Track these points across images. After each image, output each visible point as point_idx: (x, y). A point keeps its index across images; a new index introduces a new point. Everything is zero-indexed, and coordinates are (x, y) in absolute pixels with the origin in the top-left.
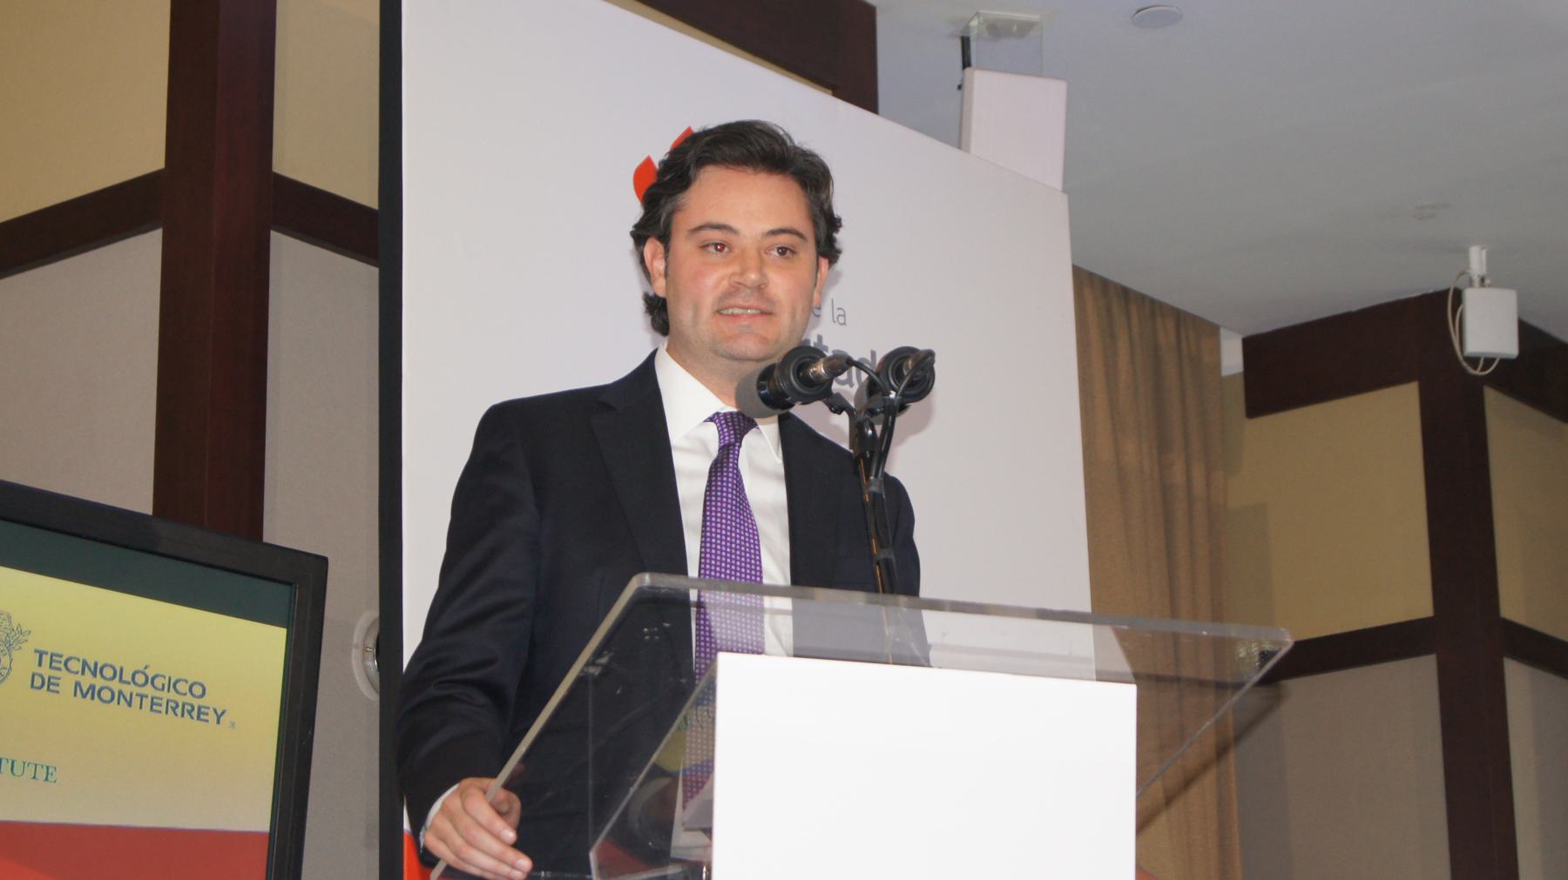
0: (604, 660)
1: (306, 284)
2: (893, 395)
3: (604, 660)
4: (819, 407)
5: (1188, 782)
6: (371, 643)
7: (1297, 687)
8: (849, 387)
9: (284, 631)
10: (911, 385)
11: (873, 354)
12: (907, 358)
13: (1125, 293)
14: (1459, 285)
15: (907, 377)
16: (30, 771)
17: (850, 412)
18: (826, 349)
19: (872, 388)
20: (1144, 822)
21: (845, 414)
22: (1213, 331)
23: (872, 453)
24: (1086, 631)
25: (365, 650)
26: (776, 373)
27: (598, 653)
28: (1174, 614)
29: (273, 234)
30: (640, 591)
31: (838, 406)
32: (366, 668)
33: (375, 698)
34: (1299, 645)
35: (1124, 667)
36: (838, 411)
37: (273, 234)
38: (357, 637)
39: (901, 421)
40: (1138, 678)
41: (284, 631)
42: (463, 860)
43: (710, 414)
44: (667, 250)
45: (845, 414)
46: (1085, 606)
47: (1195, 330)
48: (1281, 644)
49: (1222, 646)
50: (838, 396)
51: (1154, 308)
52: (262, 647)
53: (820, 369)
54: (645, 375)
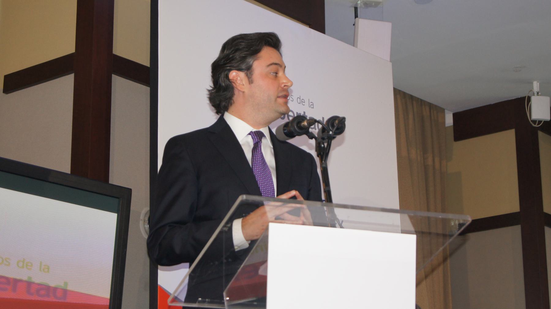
1: (123, 90)
2: (331, 133)
4: (305, 137)
6: (147, 219)
7: (473, 236)
8: (315, 130)
10: (337, 129)
12: (335, 120)
13: (412, 97)
15: (337, 126)
17: (316, 138)
19: (323, 130)
21: (314, 140)
22: (441, 111)
25: (144, 221)
26: (290, 125)
28: (428, 210)
29: (113, 75)
31: (311, 136)
32: (145, 228)
35: (412, 229)
36: (311, 138)
37: (113, 75)
38: (142, 217)
39: (334, 142)
40: (417, 233)
43: (249, 132)
45: (314, 140)
47: (436, 110)
49: (445, 222)
50: (312, 133)
51: (421, 102)
52: (110, 219)
53: (305, 123)
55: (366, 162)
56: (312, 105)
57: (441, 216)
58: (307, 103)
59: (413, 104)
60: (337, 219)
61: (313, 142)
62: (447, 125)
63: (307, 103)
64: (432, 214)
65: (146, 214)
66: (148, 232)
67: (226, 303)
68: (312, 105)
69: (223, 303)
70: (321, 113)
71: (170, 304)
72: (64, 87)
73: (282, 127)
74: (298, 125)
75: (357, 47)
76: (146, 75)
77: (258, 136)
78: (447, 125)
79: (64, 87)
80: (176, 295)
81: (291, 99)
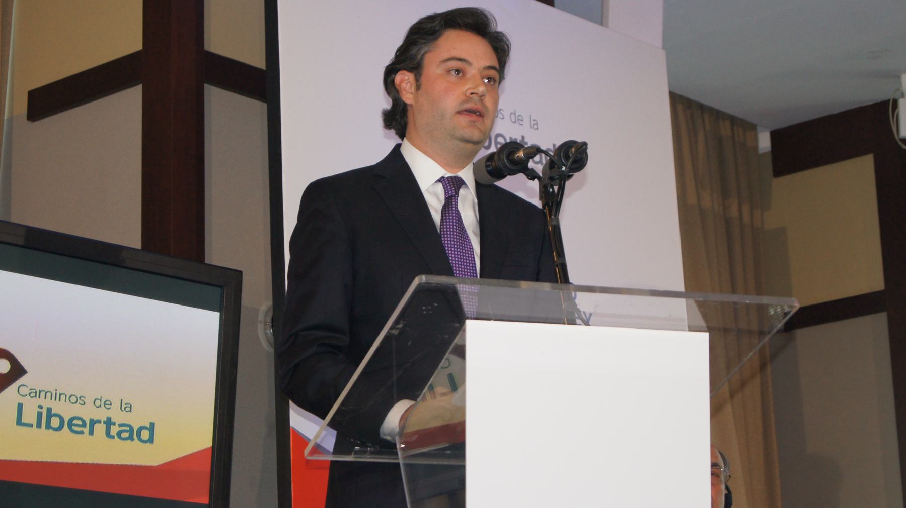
0: (400, 326)
1: (226, 114)
2: (564, 169)
3: (400, 326)
4: (521, 176)
5: (743, 385)
6: (269, 319)
7: (802, 334)
8: (537, 165)
9: (218, 314)
10: (574, 162)
11: (554, 145)
12: (571, 147)
13: (702, 107)
14: (896, 97)
15: (572, 157)
16: (43, 394)
17: (539, 179)
18: (527, 143)
19: (552, 165)
20: (716, 410)
21: (536, 181)
22: (750, 127)
23: (552, 202)
24: (683, 301)
25: (265, 323)
26: (496, 158)
27: (397, 322)
28: (734, 291)
29: (206, 85)
30: (420, 286)
31: (532, 175)
32: (266, 334)
33: (271, 350)
34: (802, 310)
35: (703, 324)
36: (532, 179)
37: (206, 85)
38: (261, 317)
39: (568, 184)
40: (710, 329)
41: (218, 314)
42: (130, 433)
43: (438, 177)
44: (417, 80)
45: (536, 181)
46: (681, 288)
47: (744, 126)
48: (792, 307)
49: (761, 309)
50: (532, 170)
51: (717, 115)
52: (205, 324)
53: (521, 154)
54: (396, 153)
55: (626, 216)
56: (535, 125)
57: (749, 300)
58: (526, 123)
59: (703, 121)
60: (579, 310)
61: (536, 183)
62: (760, 151)
63: (526, 123)
64: (735, 298)
65: (267, 312)
66: (272, 341)
67: (399, 453)
68: (535, 125)
69: (396, 454)
70: (548, 138)
71: (309, 458)
72: (126, 108)
73: (484, 161)
74: (511, 159)
75: (607, 26)
76: (260, 83)
77: (453, 185)
78: (760, 151)
79: (126, 108)
80: (318, 441)
81: (500, 115)
